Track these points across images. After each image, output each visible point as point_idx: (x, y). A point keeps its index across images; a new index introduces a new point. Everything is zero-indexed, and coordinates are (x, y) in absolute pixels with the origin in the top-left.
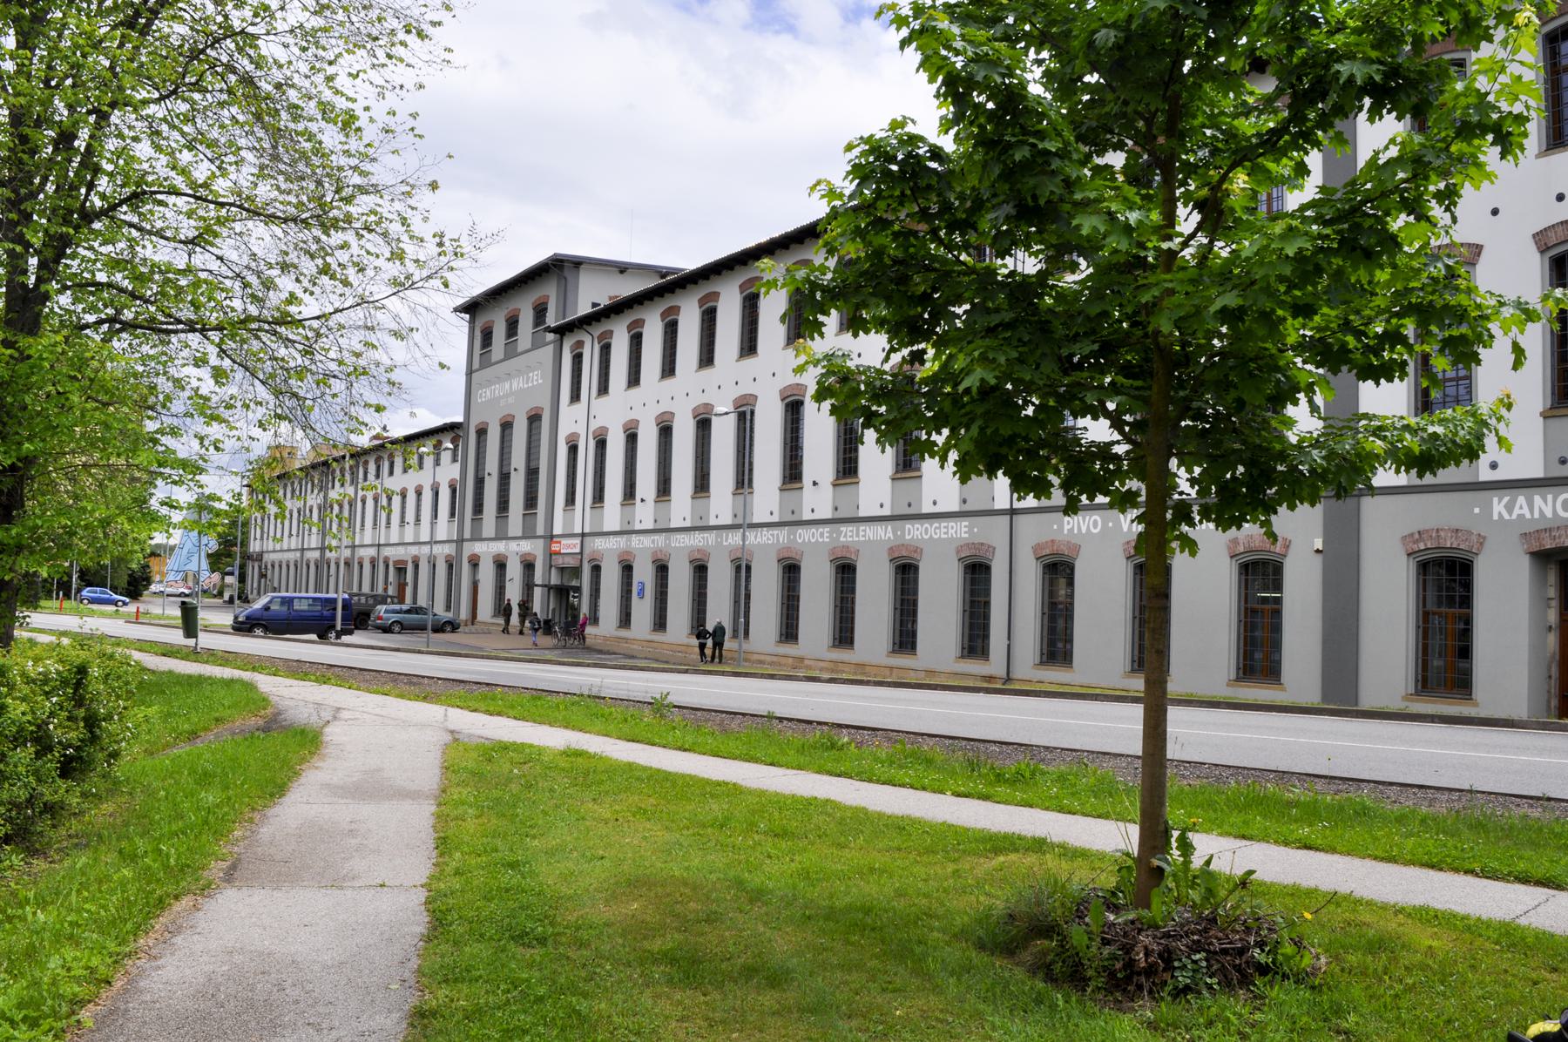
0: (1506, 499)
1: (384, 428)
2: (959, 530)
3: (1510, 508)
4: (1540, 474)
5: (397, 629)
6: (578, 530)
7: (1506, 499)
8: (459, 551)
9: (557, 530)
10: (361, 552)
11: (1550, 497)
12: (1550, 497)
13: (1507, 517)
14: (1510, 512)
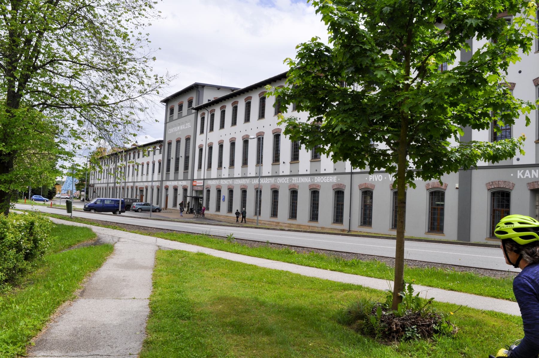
0: (522, 171)
1: (136, 142)
2: (333, 179)
3: (523, 174)
4: (534, 163)
6: (202, 178)
7: (522, 171)
8: (162, 184)
13: (522, 177)
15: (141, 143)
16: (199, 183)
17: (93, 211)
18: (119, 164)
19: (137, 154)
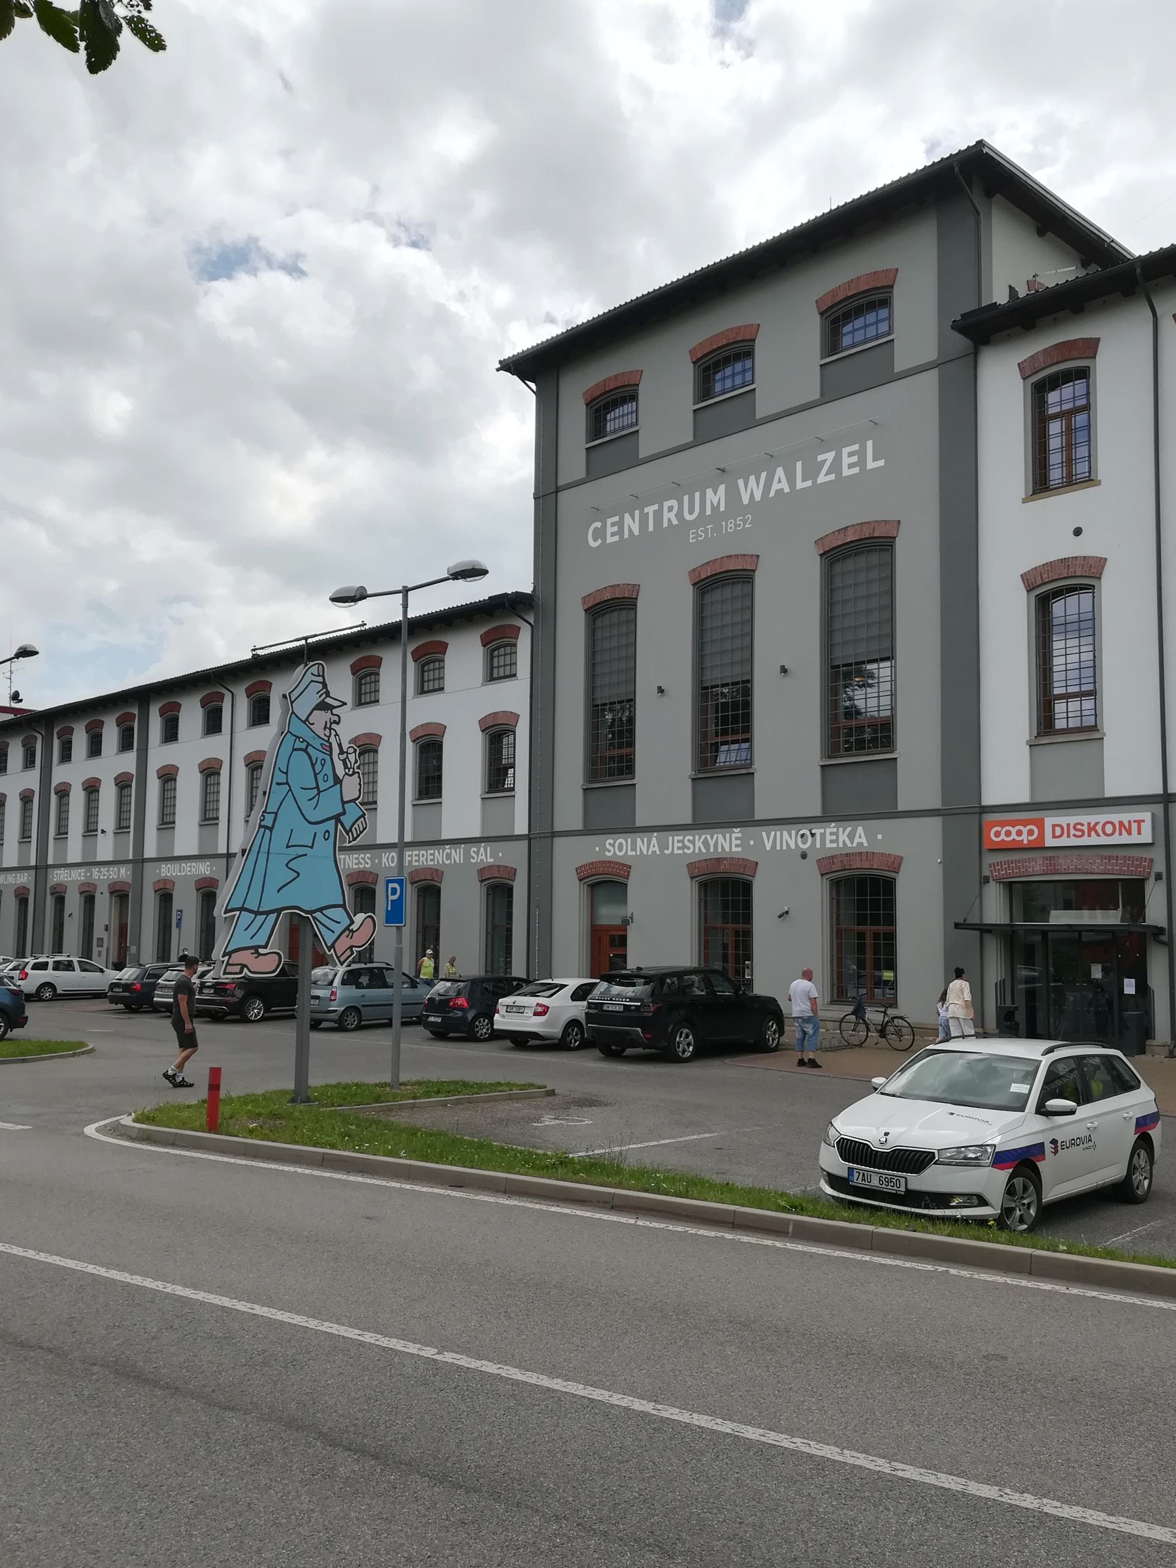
0: (849, 829)
1: (16, 697)
2: (483, 856)
3: (851, 837)
4: (79, 861)
5: (352, 1020)
6: (222, 849)
7: (849, 829)
8: (139, 876)
9: (150, 851)
10: (59, 876)
11: (793, 832)
12: (793, 832)
13: (849, 845)
14: (852, 839)
15: (38, 700)
16: (1065, 831)
17: (597, 1053)
18: (61, 774)
19: (56, 744)
